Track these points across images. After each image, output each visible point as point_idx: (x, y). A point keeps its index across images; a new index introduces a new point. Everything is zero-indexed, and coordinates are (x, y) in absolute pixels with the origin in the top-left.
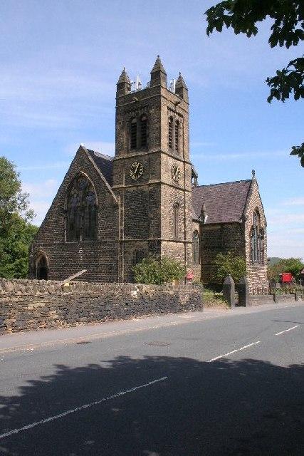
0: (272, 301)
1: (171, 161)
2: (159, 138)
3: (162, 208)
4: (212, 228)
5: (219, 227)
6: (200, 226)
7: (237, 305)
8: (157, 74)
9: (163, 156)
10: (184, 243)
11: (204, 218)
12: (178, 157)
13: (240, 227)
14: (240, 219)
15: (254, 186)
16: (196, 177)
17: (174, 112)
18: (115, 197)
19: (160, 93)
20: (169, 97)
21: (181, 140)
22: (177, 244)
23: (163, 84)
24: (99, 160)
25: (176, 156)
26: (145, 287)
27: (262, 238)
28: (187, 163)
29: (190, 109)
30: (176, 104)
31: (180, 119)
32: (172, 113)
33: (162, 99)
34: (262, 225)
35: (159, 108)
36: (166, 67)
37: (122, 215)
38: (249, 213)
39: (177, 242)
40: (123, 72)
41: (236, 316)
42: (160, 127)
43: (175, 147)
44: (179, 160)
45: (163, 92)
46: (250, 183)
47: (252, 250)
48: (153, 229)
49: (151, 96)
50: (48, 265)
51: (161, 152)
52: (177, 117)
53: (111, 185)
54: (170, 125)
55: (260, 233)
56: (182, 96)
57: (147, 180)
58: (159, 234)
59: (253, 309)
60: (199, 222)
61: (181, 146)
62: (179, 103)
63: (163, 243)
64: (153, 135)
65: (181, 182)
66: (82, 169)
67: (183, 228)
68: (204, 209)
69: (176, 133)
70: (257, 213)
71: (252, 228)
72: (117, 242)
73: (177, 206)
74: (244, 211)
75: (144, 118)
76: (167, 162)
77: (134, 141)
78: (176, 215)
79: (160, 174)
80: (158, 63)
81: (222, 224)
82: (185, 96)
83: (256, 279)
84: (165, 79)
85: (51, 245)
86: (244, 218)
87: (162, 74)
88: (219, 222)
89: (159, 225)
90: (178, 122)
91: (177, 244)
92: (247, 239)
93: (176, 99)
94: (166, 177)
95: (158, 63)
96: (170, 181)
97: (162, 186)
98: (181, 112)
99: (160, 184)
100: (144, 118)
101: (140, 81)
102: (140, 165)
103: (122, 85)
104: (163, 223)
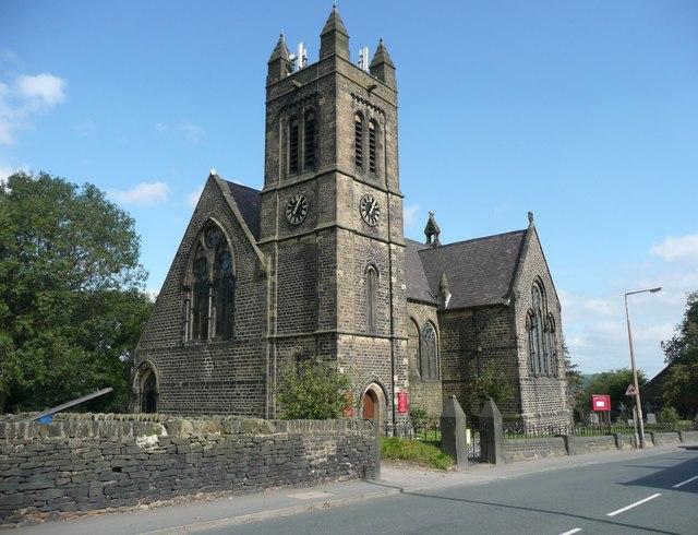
0: (562, 451)
1: (358, 189)
2: (333, 148)
3: (340, 272)
4: (458, 315)
5: (470, 314)
6: (438, 312)
7: (474, 460)
8: (330, 37)
9: (341, 178)
10: (391, 339)
11: (444, 299)
12: (378, 185)
13: (507, 311)
14: (506, 297)
15: (532, 242)
16: (437, 233)
17: (368, 104)
18: (262, 258)
19: (334, 67)
20: (355, 76)
21: (382, 154)
22: (379, 344)
23: (341, 52)
24: (241, 193)
25: (374, 183)
26: (188, 426)
27: (553, 331)
28: (392, 193)
29: (401, 101)
30: (370, 90)
31: (379, 117)
32: (361, 106)
33: (339, 79)
34: (551, 309)
35: (333, 94)
36: (348, 23)
37: (273, 289)
38: (524, 286)
39: (374, 337)
40: (280, 43)
41: (504, 482)
42: (335, 129)
43: (368, 166)
44: (377, 188)
45: (341, 67)
46: (520, 242)
47: (532, 354)
48: (323, 314)
49: (323, 74)
50: (158, 385)
51: (336, 170)
52: (373, 114)
53: (257, 240)
54: (359, 128)
55: (547, 323)
56: (382, 79)
57: (315, 224)
58: (334, 322)
59: (517, 465)
60: (436, 305)
61: (382, 165)
62: (374, 87)
63: (342, 340)
64: (324, 143)
65: (382, 229)
66: (213, 215)
67: (387, 311)
68: (445, 283)
69: (371, 141)
70: (542, 287)
71: (532, 315)
72: (264, 339)
73: (372, 271)
74: (512, 283)
75: (311, 117)
76: (349, 190)
77: (294, 156)
78: (371, 288)
79: (335, 211)
80: (333, 18)
81: (475, 309)
82: (388, 76)
83: (543, 404)
84: (345, 45)
85: (164, 349)
86: (511, 294)
87: (338, 35)
88: (470, 304)
89: (333, 306)
90: (373, 121)
91: (379, 344)
92: (521, 330)
93: (370, 82)
94: (347, 217)
95: (333, 18)
96: (357, 225)
97: (340, 232)
98: (380, 104)
99: (334, 229)
100: (311, 117)
101: (303, 54)
102: (303, 199)
103: (274, 64)
104: (341, 301)
